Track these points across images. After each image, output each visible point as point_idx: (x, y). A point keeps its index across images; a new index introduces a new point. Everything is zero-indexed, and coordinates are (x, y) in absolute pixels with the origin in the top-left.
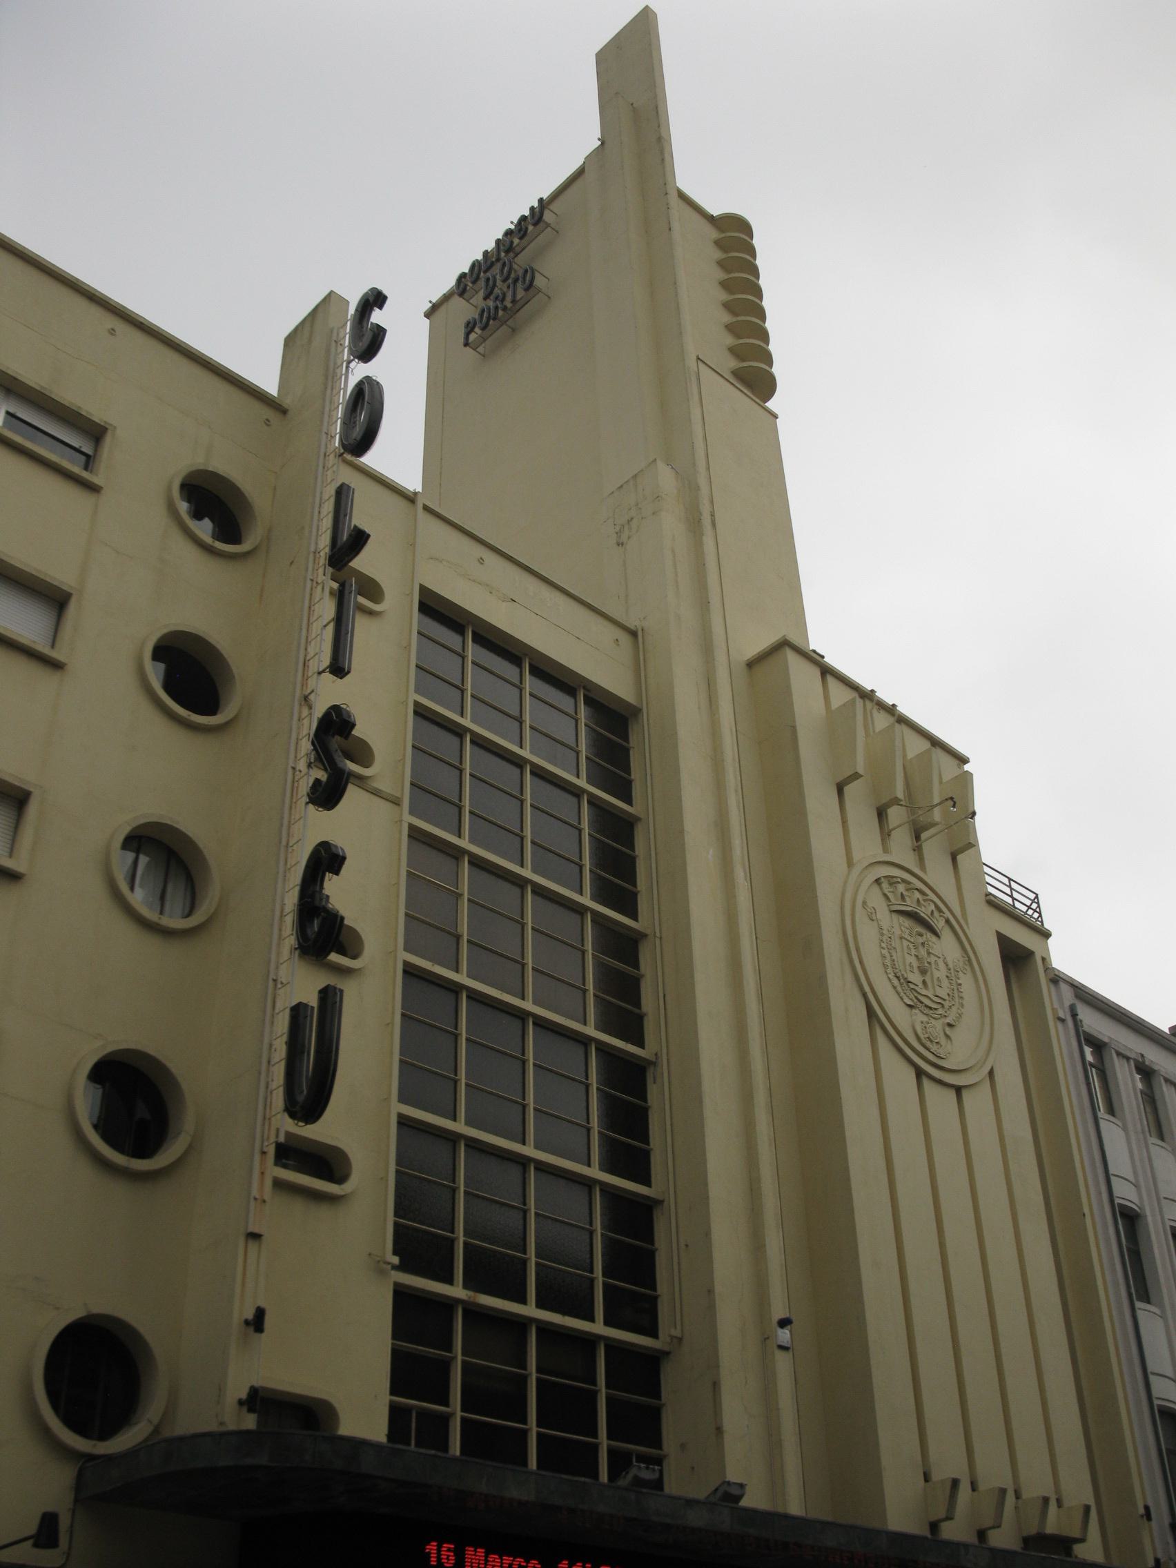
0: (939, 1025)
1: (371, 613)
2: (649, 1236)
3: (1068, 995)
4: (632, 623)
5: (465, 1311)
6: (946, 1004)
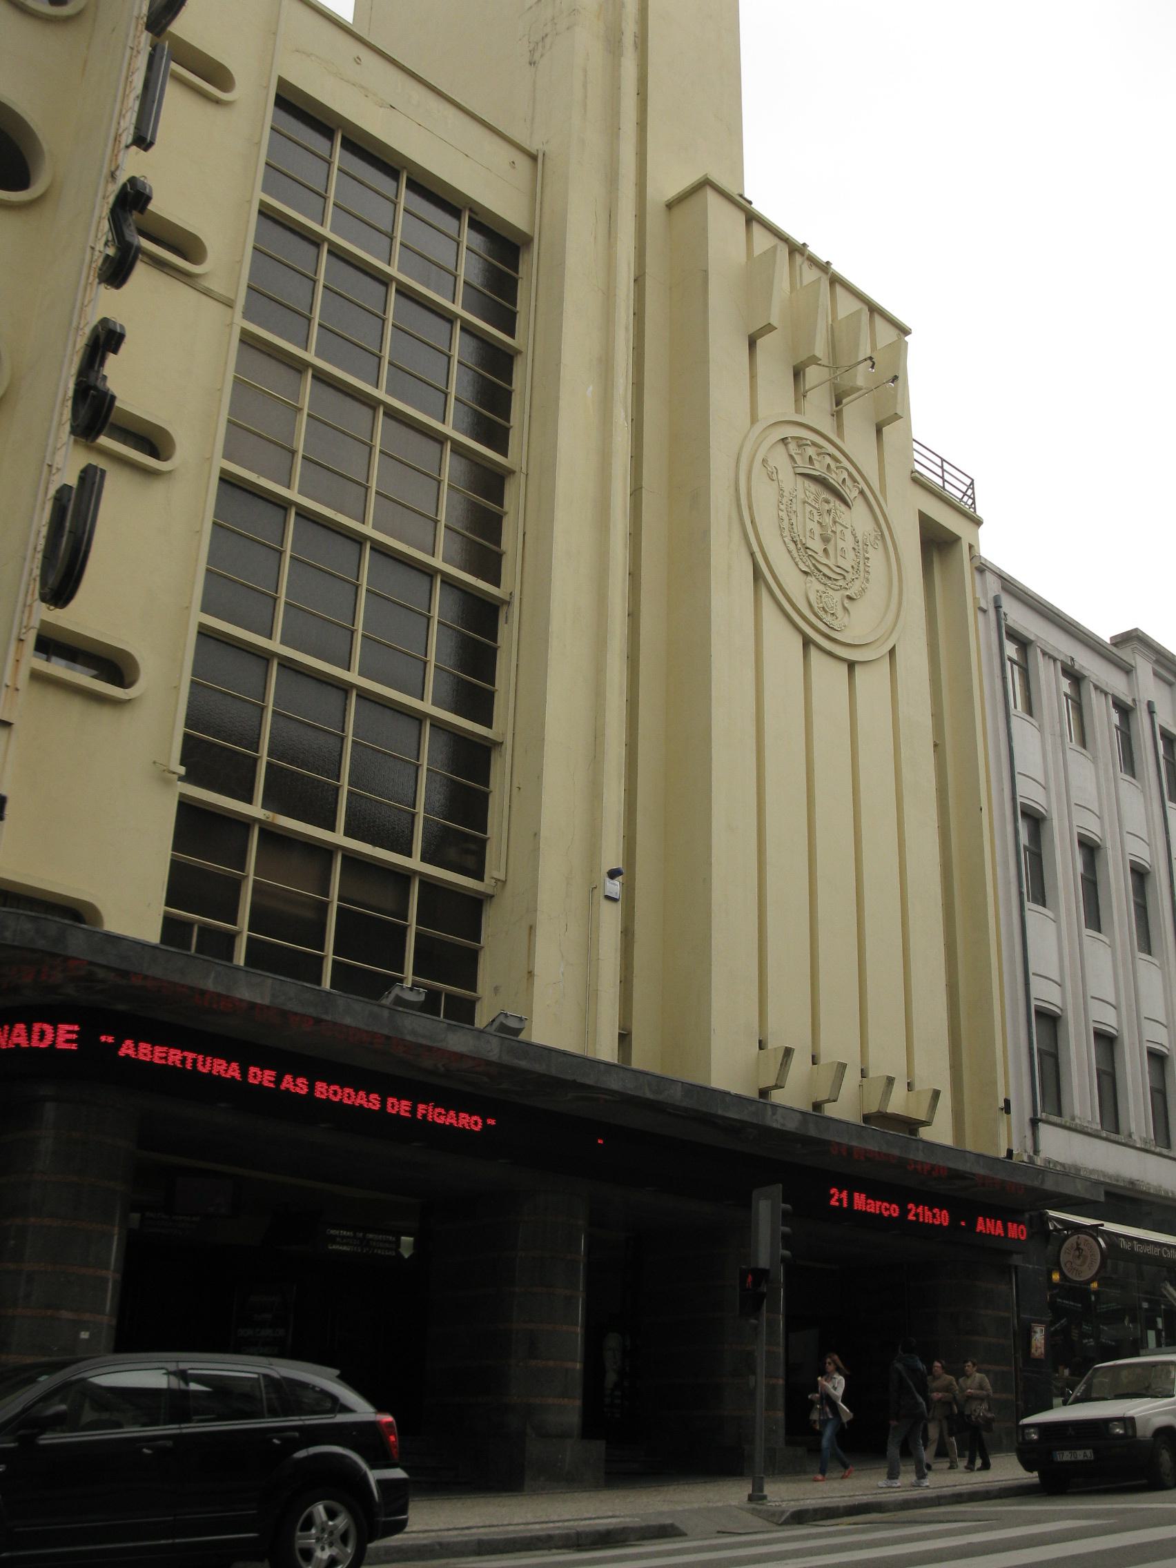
0: (837, 596)
1: (217, 102)
2: (485, 779)
3: (994, 586)
4: (533, 147)
5: (261, 831)
6: (849, 577)
